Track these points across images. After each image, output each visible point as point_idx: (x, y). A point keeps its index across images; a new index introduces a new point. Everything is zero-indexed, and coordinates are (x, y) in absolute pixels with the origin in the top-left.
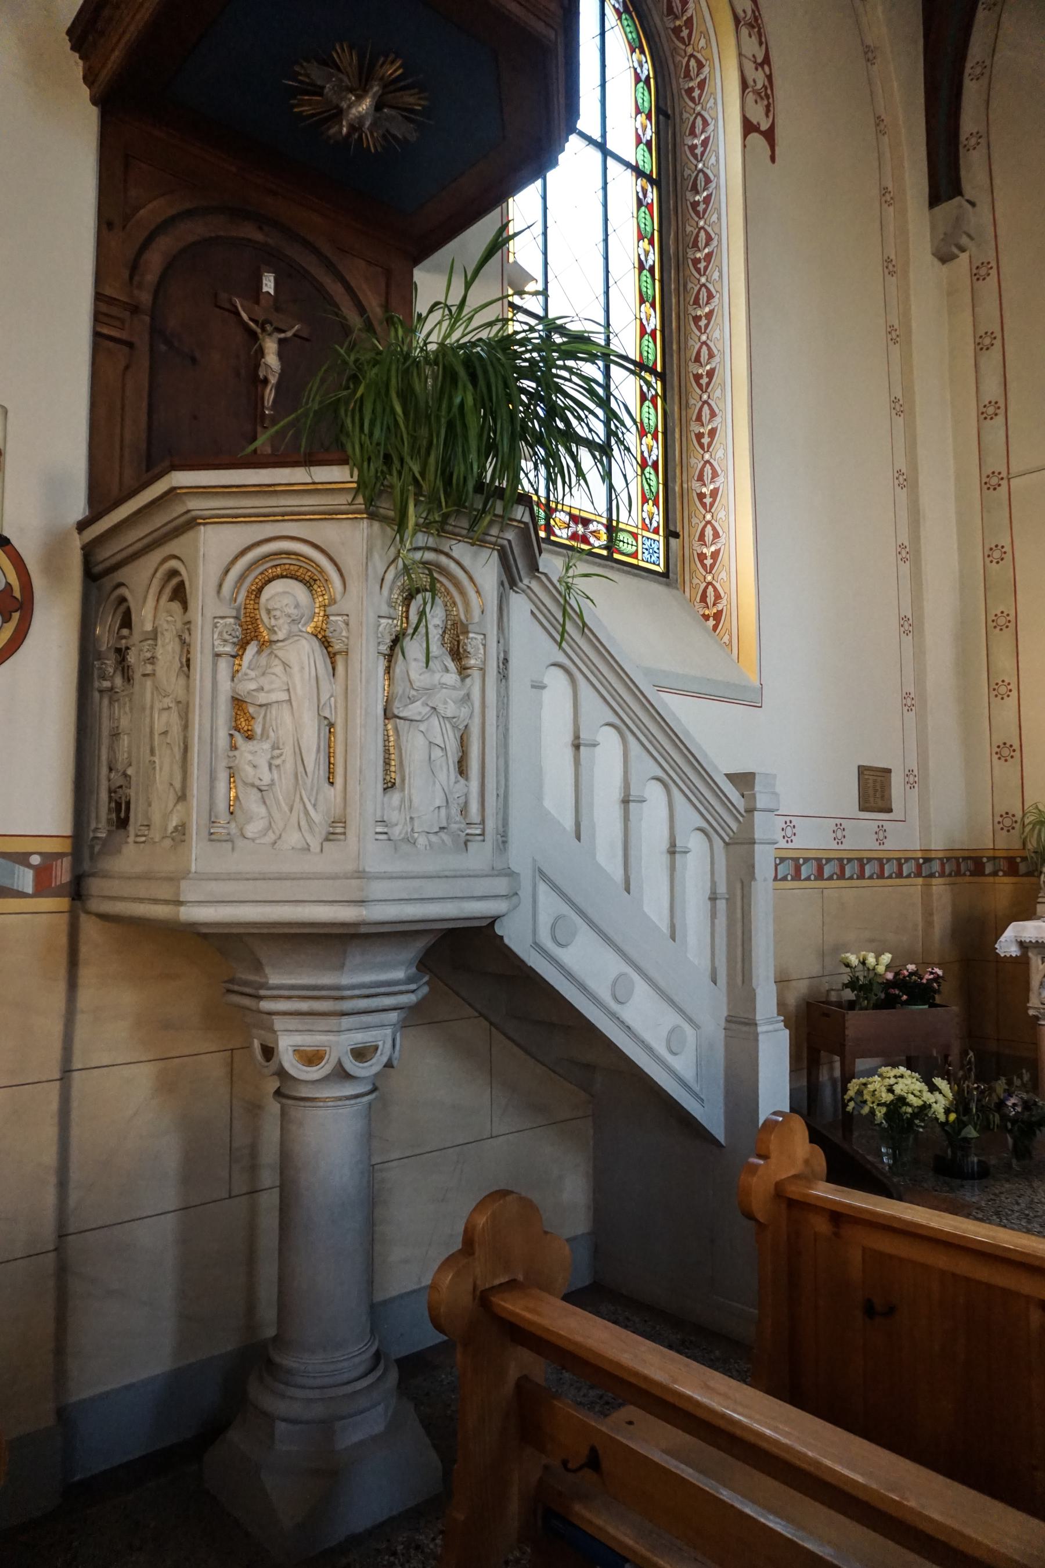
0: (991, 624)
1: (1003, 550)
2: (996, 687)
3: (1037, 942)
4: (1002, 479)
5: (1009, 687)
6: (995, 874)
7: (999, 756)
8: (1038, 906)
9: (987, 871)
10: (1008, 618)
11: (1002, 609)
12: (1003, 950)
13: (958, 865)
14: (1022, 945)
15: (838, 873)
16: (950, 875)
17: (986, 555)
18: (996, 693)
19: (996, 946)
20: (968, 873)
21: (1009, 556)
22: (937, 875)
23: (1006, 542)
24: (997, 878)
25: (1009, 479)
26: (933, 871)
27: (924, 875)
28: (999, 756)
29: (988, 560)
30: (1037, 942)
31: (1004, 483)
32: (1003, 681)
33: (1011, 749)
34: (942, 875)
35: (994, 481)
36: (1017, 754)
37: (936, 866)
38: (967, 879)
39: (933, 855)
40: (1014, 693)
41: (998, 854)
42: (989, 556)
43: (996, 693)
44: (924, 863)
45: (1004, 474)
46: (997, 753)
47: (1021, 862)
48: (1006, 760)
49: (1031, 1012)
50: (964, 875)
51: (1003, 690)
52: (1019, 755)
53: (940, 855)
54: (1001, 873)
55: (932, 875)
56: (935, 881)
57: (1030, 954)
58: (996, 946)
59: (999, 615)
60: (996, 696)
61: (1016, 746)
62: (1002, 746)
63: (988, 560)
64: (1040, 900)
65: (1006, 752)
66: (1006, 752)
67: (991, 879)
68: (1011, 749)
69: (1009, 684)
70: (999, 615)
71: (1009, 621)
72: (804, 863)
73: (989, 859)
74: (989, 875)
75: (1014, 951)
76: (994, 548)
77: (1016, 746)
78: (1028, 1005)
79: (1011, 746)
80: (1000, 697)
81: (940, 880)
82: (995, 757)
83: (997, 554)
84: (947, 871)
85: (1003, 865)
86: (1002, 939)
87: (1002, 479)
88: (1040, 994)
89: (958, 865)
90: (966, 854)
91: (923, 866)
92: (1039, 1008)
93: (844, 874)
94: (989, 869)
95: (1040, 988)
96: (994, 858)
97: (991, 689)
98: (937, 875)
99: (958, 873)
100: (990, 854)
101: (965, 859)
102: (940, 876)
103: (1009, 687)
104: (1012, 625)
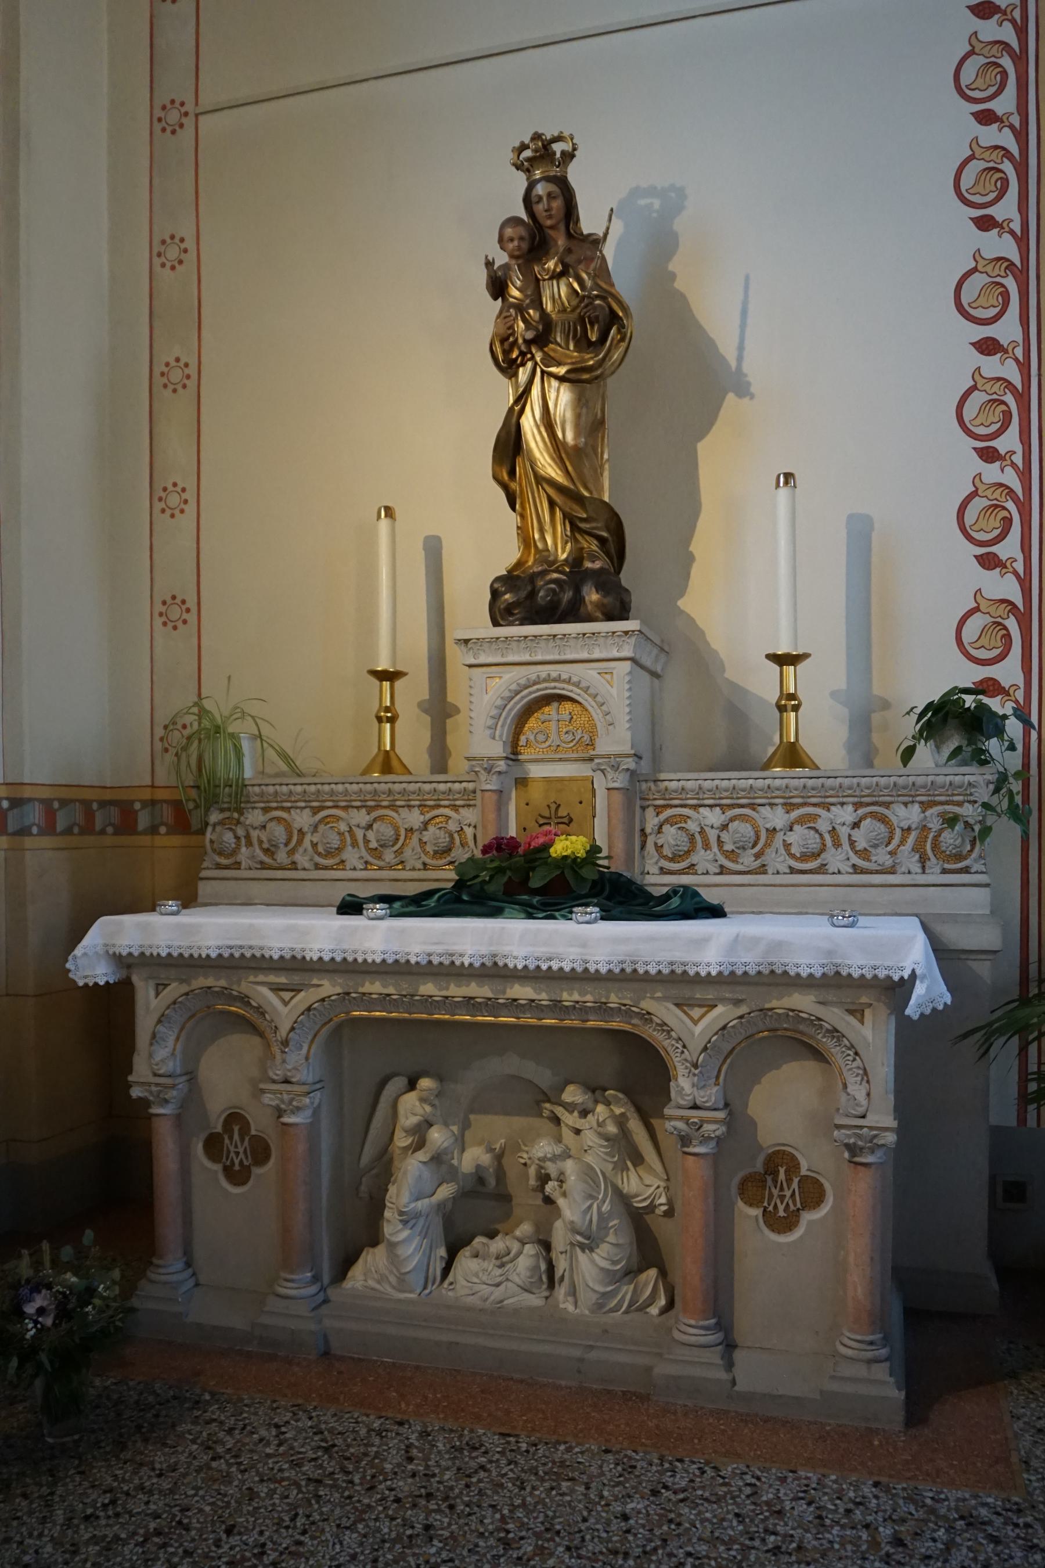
0: (159, 381)
1: (183, 246)
2: (163, 495)
3: (142, 954)
4: (186, 114)
5: (184, 496)
6: (153, 830)
7: (164, 619)
8: (201, 885)
9: (141, 827)
10: (187, 371)
11: (177, 352)
12: (80, 973)
13: (90, 815)
14: (121, 961)
15: (43, 824)
16: (68, 831)
17: (155, 253)
18: (162, 505)
19: (68, 966)
20: (110, 830)
21: (192, 254)
22: (35, 830)
23: (187, 230)
24: (157, 838)
25: (197, 115)
26: (27, 823)
27: (10, 829)
28: (164, 619)
29: (157, 261)
30: (142, 954)
31: (189, 122)
32: (175, 485)
33: (184, 607)
34: (49, 828)
35: (173, 117)
36: (192, 618)
37: (34, 815)
38: (109, 840)
39: (27, 792)
40: (191, 509)
41: (161, 795)
42: (159, 255)
43: (162, 505)
44: (60, 808)
45: (189, 107)
46: (161, 614)
47: (143, 808)
48: (175, 628)
49: (136, 1092)
50: (103, 832)
51: (174, 500)
52: (195, 617)
53: (45, 794)
54: (163, 830)
55: (24, 832)
56: (28, 842)
57: (135, 979)
58: (68, 966)
59: (173, 363)
60: (163, 511)
61: (192, 603)
62: (178, 601)
63: (157, 261)
64: (204, 874)
65: (175, 613)
66: (175, 613)
67: (145, 840)
68: (184, 607)
69: (184, 490)
70: (173, 363)
71: (188, 377)
72: (60, 808)
73: (145, 804)
74: (144, 833)
75: (101, 973)
76: (169, 241)
77: (192, 603)
78: (130, 1078)
79: (184, 602)
80: (168, 512)
81: (46, 841)
82: (158, 621)
83: (173, 253)
84: (61, 825)
85: (167, 813)
86: (78, 951)
87: (186, 114)
88: (151, 1056)
89: (90, 815)
90: (108, 796)
91: (10, 814)
92: (149, 1084)
93: (54, 828)
94: (143, 820)
95: (151, 1044)
96: (153, 803)
97: (155, 499)
98: (35, 830)
99: (88, 829)
100: (147, 795)
101: (103, 804)
102: (42, 833)
103: (184, 496)
104: (192, 384)
